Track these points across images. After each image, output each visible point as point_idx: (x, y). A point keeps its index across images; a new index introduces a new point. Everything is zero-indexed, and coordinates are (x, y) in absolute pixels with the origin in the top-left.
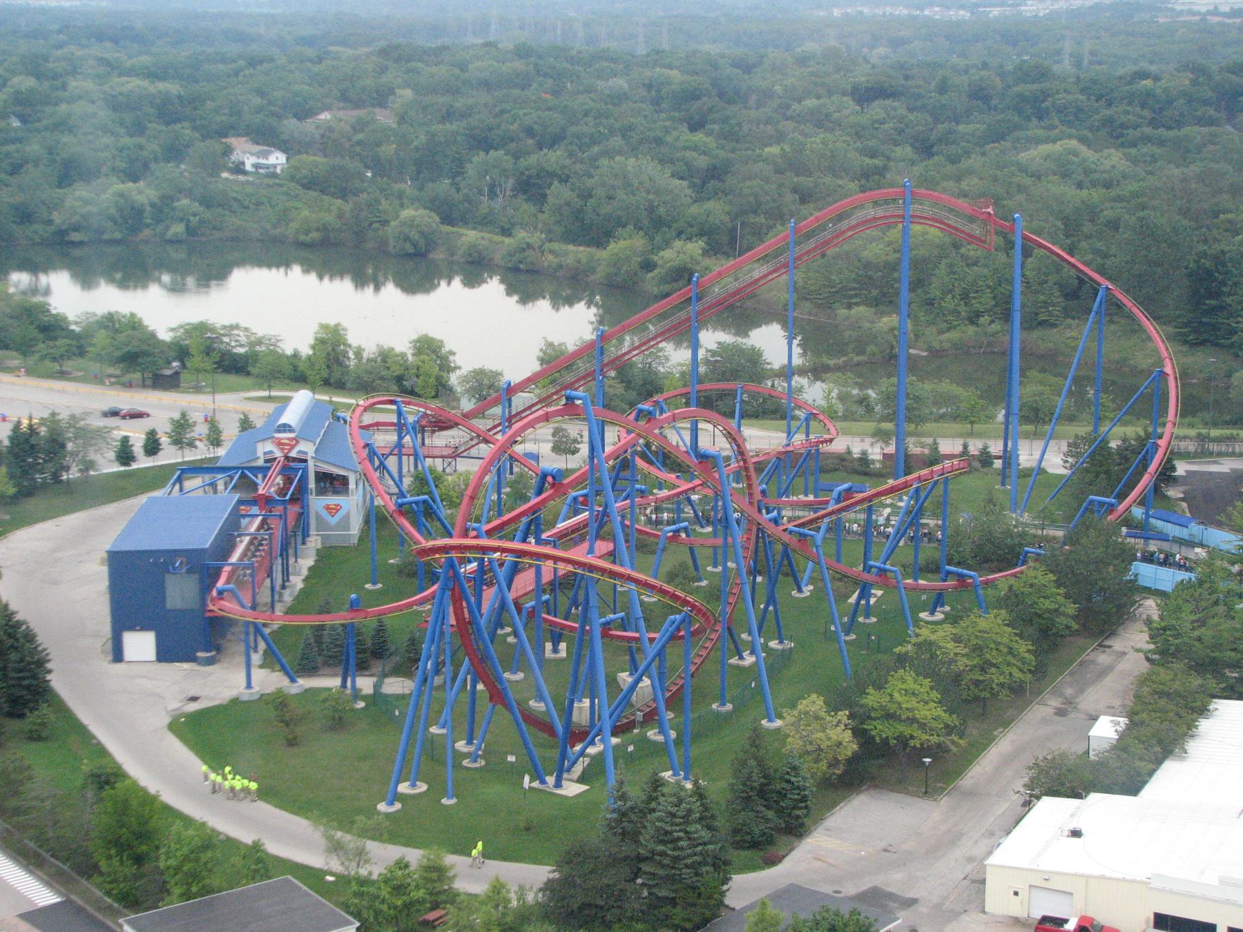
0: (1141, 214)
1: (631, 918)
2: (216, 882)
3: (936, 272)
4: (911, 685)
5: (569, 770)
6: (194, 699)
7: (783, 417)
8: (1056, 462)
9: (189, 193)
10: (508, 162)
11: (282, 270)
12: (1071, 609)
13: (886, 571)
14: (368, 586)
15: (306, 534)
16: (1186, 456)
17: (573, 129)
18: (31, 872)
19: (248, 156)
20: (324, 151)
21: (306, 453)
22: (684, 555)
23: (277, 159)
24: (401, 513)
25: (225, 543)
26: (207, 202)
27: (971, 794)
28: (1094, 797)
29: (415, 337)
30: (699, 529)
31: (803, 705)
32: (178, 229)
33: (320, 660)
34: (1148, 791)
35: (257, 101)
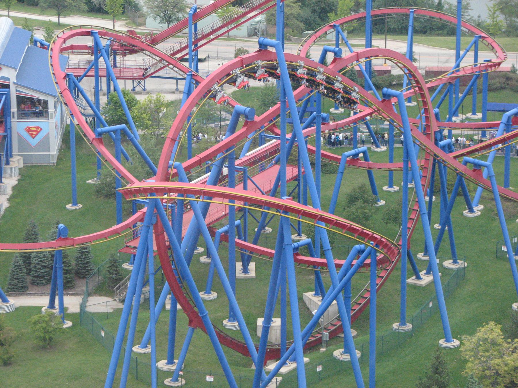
7: (452, 32)
14: (69, 206)
21: (8, 79)
22: (363, 179)
24: (100, 141)
30: (374, 148)
31: (482, 332)
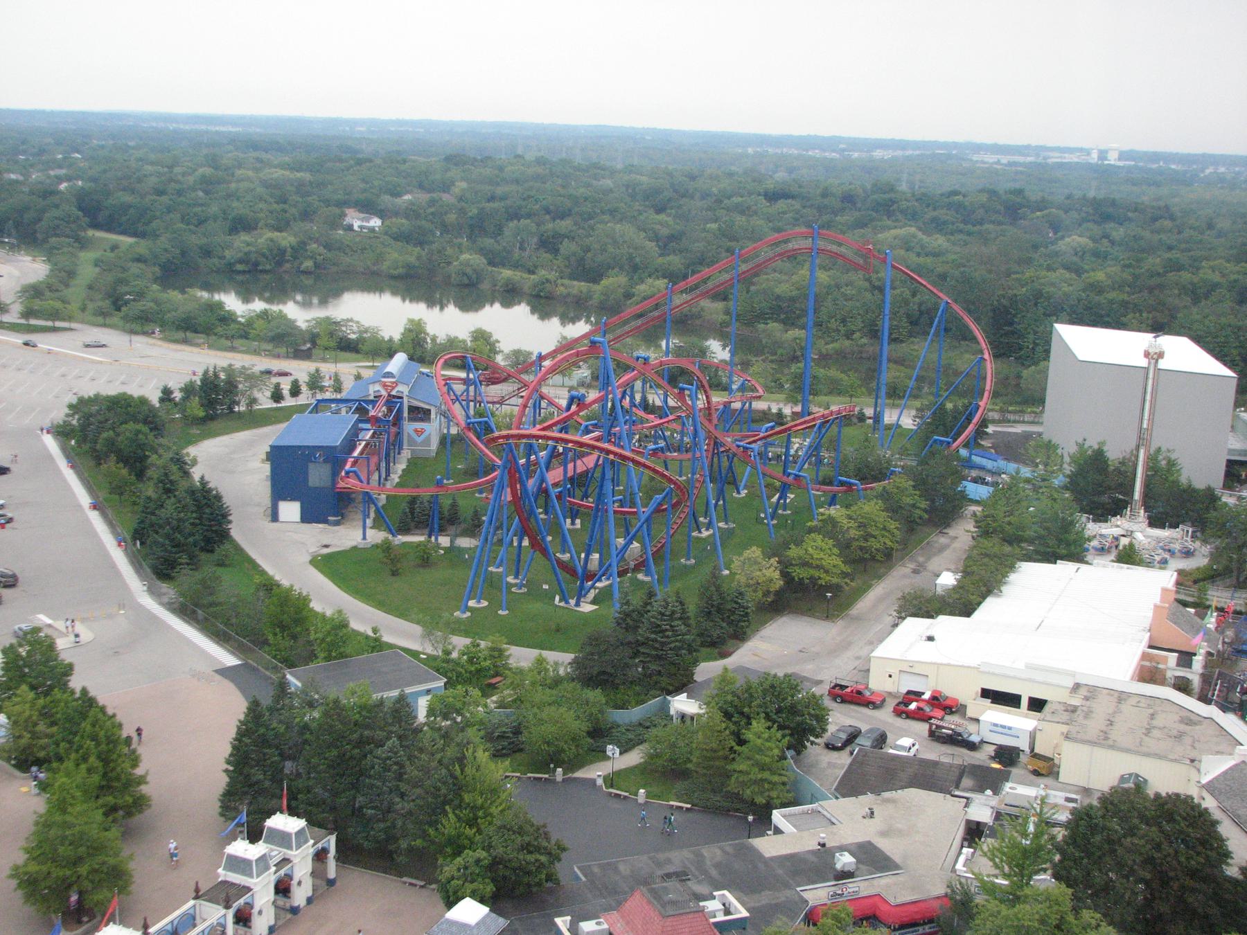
0: (962, 269)
1: (631, 683)
2: (348, 650)
3: (825, 304)
4: (819, 543)
5: (585, 596)
6: (326, 546)
8: (908, 421)
9: (317, 241)
10: (533, 227)
11: (377, 295)
12: (924, 504)
13: (799, 476)
15: (400, 448)
16: (994, 422)
17: (577, 209)
18: (221, 646)
19: (356, 220)
20: (407, 218)
23: (376, 222)
24: (469, 429)
25: (350, 443)
26: (328, 247)
27: (857, 619)
28: (941, 618)
29: (473, 329)
31: (747, 554)
32: (308, 264)
33: (413, 524)
34: (977, 614)
35: (362, 186)
